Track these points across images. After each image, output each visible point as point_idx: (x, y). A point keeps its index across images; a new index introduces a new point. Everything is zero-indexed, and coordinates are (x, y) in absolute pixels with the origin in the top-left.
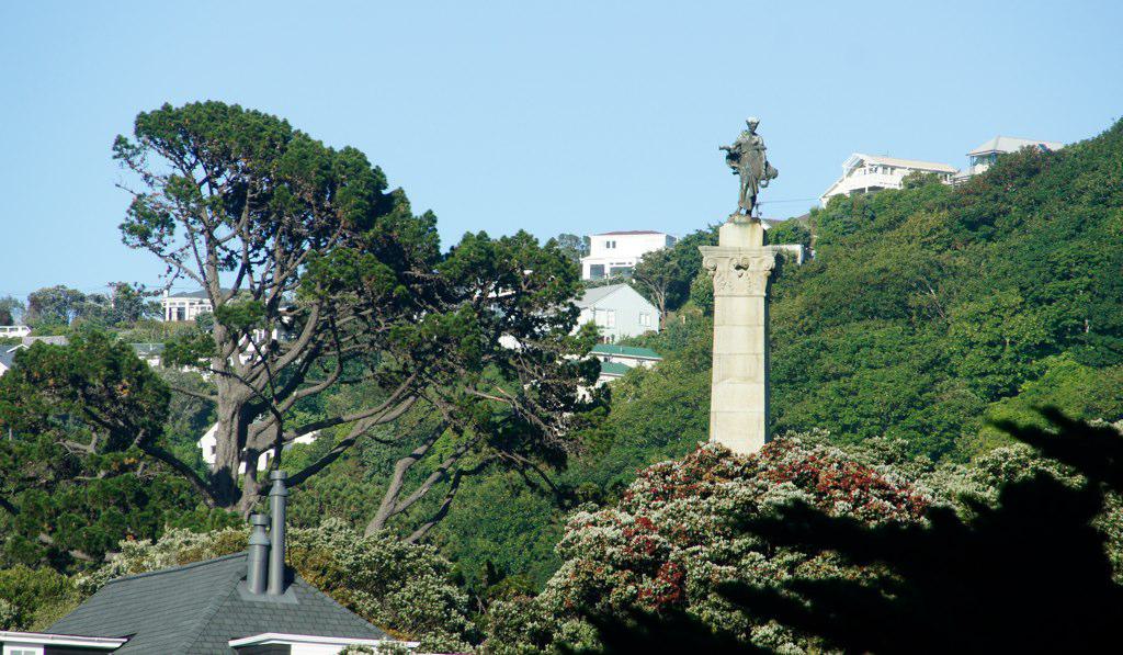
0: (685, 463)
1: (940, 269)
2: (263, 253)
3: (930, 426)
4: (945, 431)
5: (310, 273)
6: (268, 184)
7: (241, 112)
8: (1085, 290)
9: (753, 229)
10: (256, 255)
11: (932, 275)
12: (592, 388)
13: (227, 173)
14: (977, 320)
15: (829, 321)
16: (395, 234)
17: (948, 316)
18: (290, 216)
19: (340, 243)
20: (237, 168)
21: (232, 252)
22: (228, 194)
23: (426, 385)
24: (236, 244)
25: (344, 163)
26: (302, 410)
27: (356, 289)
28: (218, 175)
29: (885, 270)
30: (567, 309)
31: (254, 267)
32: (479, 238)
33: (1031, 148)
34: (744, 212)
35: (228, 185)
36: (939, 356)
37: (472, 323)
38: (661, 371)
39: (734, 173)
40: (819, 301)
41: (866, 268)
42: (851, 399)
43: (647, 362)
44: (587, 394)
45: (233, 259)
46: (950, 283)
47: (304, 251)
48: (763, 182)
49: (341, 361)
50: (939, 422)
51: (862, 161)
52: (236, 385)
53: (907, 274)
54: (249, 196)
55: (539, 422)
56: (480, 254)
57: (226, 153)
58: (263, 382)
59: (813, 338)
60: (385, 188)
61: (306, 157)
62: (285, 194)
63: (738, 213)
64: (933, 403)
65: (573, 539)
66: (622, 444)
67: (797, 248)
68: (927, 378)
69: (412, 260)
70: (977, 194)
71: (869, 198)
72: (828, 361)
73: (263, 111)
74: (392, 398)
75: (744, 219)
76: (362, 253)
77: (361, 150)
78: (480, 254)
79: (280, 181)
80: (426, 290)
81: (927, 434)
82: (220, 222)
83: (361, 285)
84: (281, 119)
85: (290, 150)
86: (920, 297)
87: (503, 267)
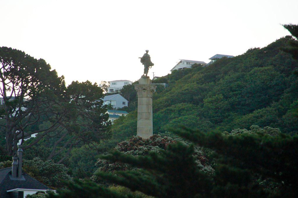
8: (240, 94)
12: (107, 122)
21: (10, 87)
24: (11, 85)
30: (100, 101)
31: (16, 91)
33: (57, 73)
44: (105, 123)
48: (150, 67)
53: (193, 91)
59: (168, 108)
60: (51, 69)
65: (100, 162)
84: (59, 75)
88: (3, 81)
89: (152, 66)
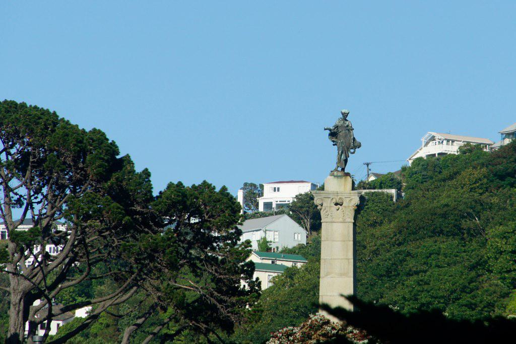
0: (301, 329)
1: (482, 205)
2: (40, 197)
3: (475, 305)
4: (485, 307)
5: (70, 209)
6: (43, 152)
7: (27, 107)
9: (346, 180)
10: (36, 198)
11: (478, 208)
13: (17, 146)
14: (505, 237)
15: (412, 237)
16: (124, 183)
17: (486, 234)
18: (57, 173)
19: (88, 190)
20: (23, 142)
21: (21, 196)
22: (18, 159)
23: (144, 279)
24: (23, 191)
25: (92, 139)
26: (80, 296)
27: (99, 218)
28: (12, 147)
29: (447, 205)
30: (233, 231)
31: (35, 205)
32: (177, 186)
34: (340, 169)
35: (18, 154)
36: (481, 259)
37: (173, 240)
38: (306, 269)
39: (334, 145)
40: (405, 225)
41: (435, 204)
42: (426, 287)
43: (299, 263)
44: (247, 285)
45: (21, 201)
46: (487, 213)
47: (67, 194)
48: (352, 151)
49: (90, 265)
50: (481, 302)
51: (434, 137)
52: (22, 280)
53: (461, 208)
54: (31, 160)
55: (216, 302)
56: (178, 196)
57: (17, 132)
58: (40, 279)
59: (402, 248)
61: (67, 135)
62: (54, 159)
63: (336, 170)
64: (478, 289)
66: (282, 316)
67: (393, 191)
68: (473, 274)
69: (135, 200)
70: (504, 158)
71: (438, 159)
72: (411, 264)
73: (40, 106)
74: (122, 288)
75: (340, 174)
76: (103, 196)
77: (103, 131)
78: (178, 196)
79: (51, 151)
80: (144, 219)
81: (473, 309)
82: (12, 177)
83: (103, 216)
84: (51, 111)
85: (57, 131)
86: (469, 222)
87: (192, 204)
88: (5, 183)
89: (357, 149)
